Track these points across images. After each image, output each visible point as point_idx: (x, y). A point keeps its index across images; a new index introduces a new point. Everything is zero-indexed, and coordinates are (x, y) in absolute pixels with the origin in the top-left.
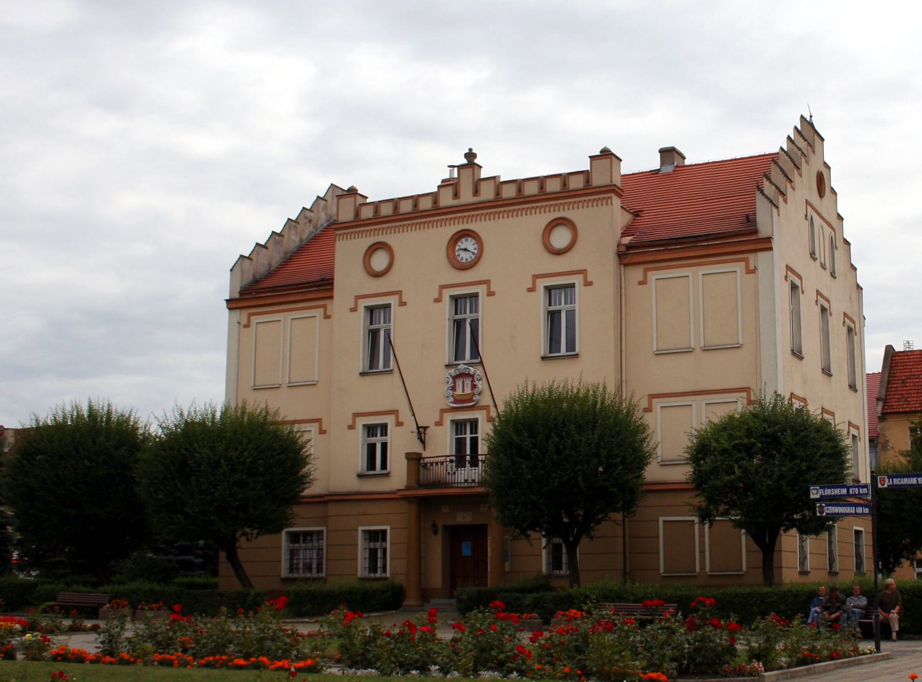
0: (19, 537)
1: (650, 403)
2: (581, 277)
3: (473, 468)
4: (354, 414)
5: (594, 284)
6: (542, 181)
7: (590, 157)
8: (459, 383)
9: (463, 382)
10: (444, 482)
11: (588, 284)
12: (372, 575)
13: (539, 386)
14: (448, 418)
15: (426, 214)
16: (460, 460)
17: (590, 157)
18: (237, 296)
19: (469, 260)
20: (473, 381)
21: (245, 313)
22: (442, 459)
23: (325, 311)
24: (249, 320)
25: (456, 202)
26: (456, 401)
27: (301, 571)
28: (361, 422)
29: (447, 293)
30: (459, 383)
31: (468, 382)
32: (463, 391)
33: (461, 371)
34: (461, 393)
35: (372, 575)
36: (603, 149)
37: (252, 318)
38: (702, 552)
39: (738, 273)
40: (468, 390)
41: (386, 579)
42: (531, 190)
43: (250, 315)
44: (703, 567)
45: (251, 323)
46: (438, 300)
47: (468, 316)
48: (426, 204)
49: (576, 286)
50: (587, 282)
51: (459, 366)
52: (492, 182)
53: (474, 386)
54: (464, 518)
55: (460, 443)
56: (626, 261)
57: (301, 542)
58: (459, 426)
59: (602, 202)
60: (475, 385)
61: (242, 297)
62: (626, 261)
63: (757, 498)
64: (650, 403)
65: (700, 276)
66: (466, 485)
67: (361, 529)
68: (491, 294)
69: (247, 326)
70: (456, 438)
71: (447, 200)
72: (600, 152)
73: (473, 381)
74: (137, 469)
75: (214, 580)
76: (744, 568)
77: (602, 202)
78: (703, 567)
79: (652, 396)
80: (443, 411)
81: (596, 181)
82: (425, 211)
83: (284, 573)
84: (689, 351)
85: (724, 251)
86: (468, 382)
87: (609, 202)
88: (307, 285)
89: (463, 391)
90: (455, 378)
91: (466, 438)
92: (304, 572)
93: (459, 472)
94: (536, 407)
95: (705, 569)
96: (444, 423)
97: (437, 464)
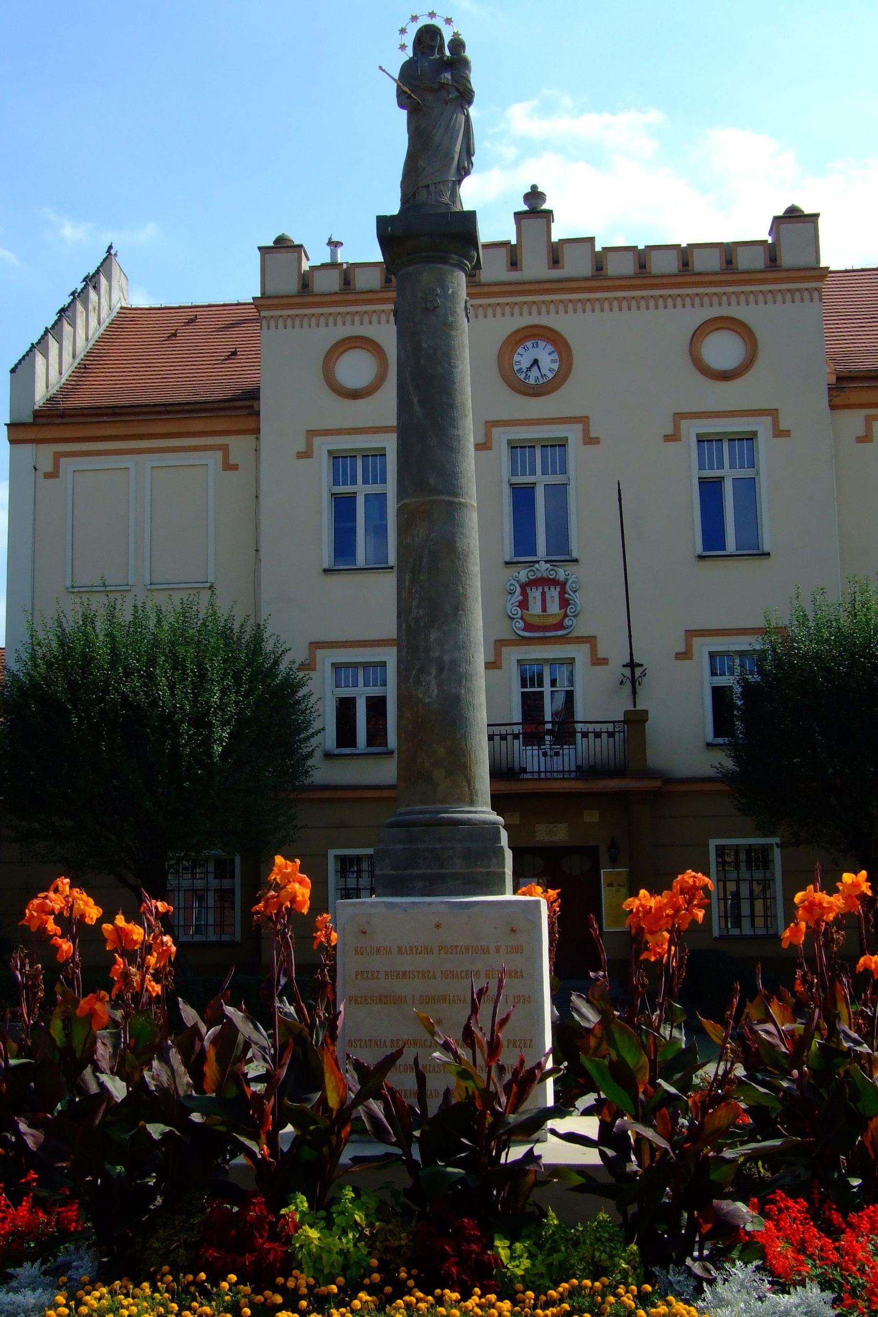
2: (768, 420)
3: (530, 748)
4: (311, 643)
7: (260, 248)
8: (535, 594)
9: (543, 594)
17: (260, 248)
20: (563, 592)
21: (47, 451)
23: (226, 456)
24: (56, 465)
29: (323, 446)
30: (535, 594)
31: (554, 593)
32: (544, 609)
33: (539, 575)
36: (279, 237)
40: (554, 608)
41: (232, 944)
43: (58, 456)
45: (62, 469)
47: (541, 481)
50: (590, 438)
51: (537, 565)
53: (564, 603)
56: (837, 401)
59: (302, 321)
62: (837, 401)
63: (49, 821)
67: (332, 853)
69: (54, 474)
70: (523, 693)
72: (274, 242)
73: (563, 592)
75: (459, 947)
77: (302, 321)
79: (316, 645)
81: (787, 259)
82: (662, 276)
86: (554, 593)
87: (816, 295)
88: (187, 407)
89: (544, 609)
91: (543, 692)
93: (566, 752)
94: (87, 660)
96: (318, 666)
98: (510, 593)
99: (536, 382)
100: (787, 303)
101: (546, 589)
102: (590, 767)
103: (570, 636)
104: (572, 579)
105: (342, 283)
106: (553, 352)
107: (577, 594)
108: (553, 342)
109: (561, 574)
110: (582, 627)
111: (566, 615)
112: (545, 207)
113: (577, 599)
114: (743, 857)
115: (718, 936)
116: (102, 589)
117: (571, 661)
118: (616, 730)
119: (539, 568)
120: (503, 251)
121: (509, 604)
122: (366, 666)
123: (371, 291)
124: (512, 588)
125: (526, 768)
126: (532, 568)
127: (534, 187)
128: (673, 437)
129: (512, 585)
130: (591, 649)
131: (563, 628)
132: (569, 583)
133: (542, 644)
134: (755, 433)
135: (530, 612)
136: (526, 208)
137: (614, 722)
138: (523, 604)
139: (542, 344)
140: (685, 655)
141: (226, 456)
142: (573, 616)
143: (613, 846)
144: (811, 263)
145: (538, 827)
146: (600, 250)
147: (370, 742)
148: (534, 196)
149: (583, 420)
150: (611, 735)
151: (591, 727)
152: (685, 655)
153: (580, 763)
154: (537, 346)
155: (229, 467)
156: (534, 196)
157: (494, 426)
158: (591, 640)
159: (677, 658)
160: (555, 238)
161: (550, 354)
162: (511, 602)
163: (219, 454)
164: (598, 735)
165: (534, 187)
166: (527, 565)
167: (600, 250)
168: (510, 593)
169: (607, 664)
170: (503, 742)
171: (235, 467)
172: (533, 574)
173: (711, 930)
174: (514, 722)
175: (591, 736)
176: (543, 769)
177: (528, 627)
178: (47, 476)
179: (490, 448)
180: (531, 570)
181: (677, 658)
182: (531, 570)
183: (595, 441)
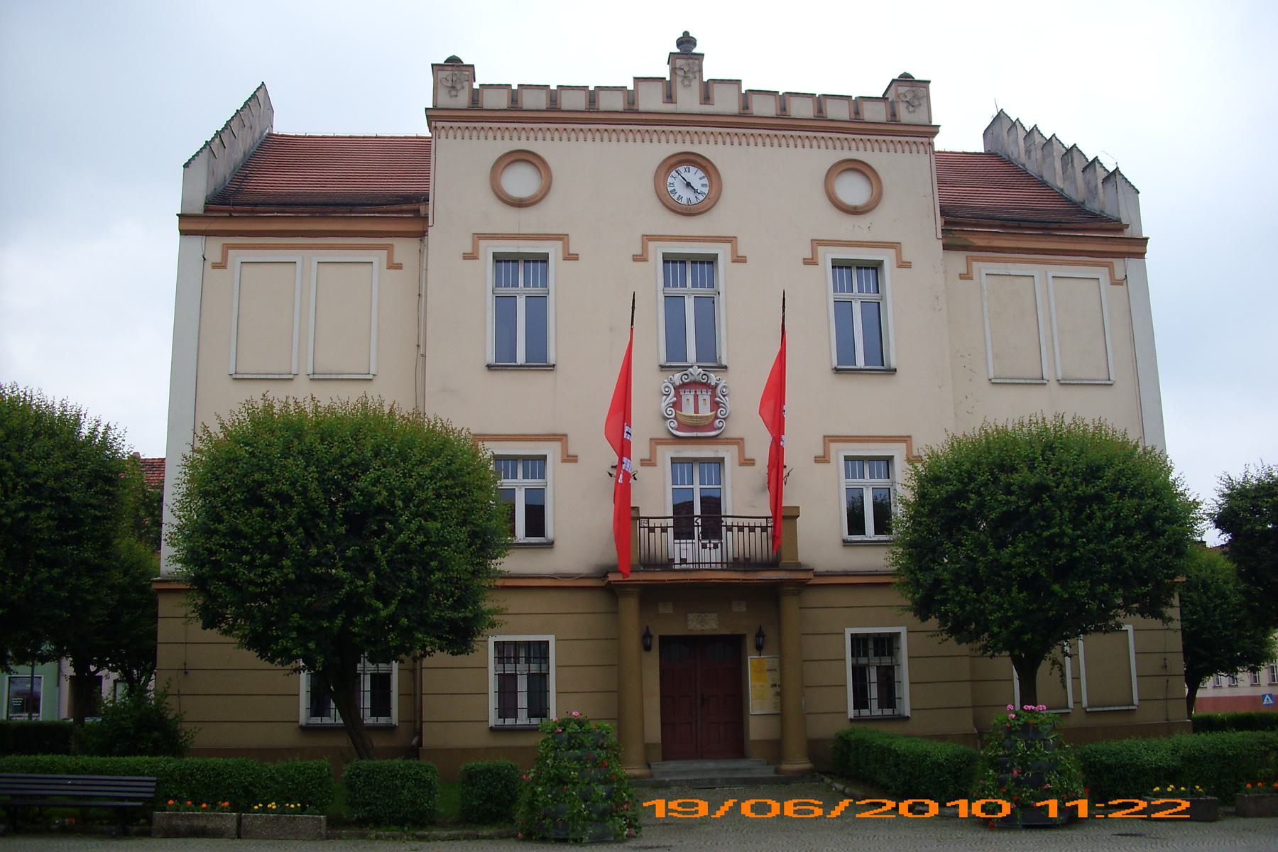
0: (310, 644)
2: (559, 244)
6: (820, 101)
8: (688, 397)
9: (696, 397)
12: (317, 720)
13: (226, 418)
16: (683, 528)
18: (198, 208)
19: (684, 201)
20: (714, 395)
21: (215, 245)
22: (752, 522)
24: (225, 256)
25: (669, 107)
27: (875, 704)
30: (688, 397)
31: (705, 397)
32: (696, 411)
35: (317, 720)
37: (231, 252)
38: (1076, 678)
40: (705, 411)
42: (803, 110)
43: (227, 248)
44: (1078, 702)
46: (640, 258)
49: (887, 266)
53: (715, 405)
54: (705, 624)
57: (871, 652)
60: (718, 403)
65: (315, 265)
66: (684, 566)
68: (739, 259)
71: (652, 101)
73: (714, 395)
76: (1136, 701)
78: (1078, 702)
80: (656, 442)
82: (563, 111)
83: (493, 720)
84: (1040, 383)
86: (705, 397)
89: (696, 411)
90: (684, 385)
92: (880, 706)
95: (1081, 703)
96: (659, 462)
97: (741, 529)
98: (665, 395)
99: (688, 203)
100: (750, 146)
101: (699, 393)
102: (745, 559)
103: (720, 437)
105: (510, 101)
106: (703, 177)
107: (726, 398)
109: (713, 379)
111: (716, 417)
112: (695, 51)
114: (871, 645)
115: (853, 717)
117: (544, 458)
118: (769, 525)
119: (693, 373)
120: (659, 85)
121: (663, 405)
122: (525, 459)
123: (538, 111)
124: (667, 389)
125: (686, 559)
126: (685, 372)
127: (686, 34)
128: (811, 261)
129: (667, 387)
130: (907, 447)
131: (715, 429)
132: (719, 388)
133: (692, 444)
134: (880, 263)
135: (682, 413)
136: (678, 51)
137: (767, 518)
138: (677, 405)
139: (693, 169)
140: (822, 459)
141: (390, 256)
142: (723, 419)
143: (760, 634)
144: (925, 121)
145: (691, 616)
146: (593, 89)
147: (529, 533)
148: (686, 41)
150: (764, 529)
152: (822, 459)
153: (736, 556)
154: (689, 171)
156: (686, 41)
158: (738, 442)
159: (816, 461)
160: (705, 79)
161: (700, 179)
162: (666, 403)
164: (752, 529)
165: (686, 34)
166: (681, 369)
167: (593, 89)
168: (665, 395)
169: (753, 464)
170: (741, 533)
171: (399, 267)
172: (686, 377)
173: (846, 712)
174: (668, 516)
175: (746, 530)
176: (725, 561)
178: (216, 266)
179: (476, 258)
180: (685, 374)
181: (816, 461)
182: (685, 374)
183: (575, 257)
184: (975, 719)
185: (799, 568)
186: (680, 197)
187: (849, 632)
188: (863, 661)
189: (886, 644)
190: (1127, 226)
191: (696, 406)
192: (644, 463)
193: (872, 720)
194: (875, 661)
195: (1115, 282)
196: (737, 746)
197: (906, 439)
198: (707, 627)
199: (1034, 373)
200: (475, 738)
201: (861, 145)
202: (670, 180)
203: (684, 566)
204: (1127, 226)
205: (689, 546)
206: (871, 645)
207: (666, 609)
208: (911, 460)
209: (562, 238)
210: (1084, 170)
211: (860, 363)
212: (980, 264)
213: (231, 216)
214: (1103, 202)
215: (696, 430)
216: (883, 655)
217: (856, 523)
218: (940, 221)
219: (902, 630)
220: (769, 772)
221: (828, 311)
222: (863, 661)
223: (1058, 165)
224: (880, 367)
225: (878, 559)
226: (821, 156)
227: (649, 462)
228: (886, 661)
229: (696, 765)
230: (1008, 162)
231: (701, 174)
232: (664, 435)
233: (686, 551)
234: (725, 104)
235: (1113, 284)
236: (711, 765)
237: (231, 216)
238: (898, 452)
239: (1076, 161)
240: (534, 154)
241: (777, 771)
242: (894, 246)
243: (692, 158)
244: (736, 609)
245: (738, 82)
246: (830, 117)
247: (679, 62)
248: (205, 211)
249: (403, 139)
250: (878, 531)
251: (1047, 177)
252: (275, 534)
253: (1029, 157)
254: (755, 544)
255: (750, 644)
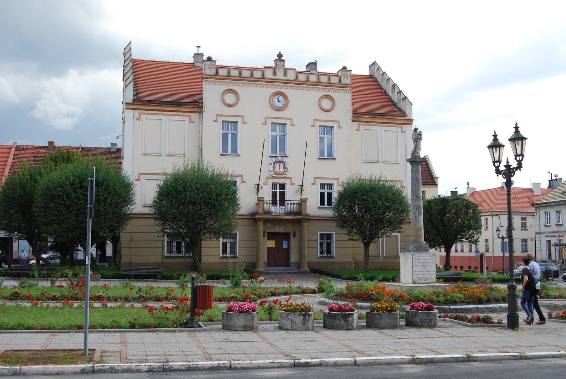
1: (139, 177)
5: (343, 128)
8: (277, 165)
9: (279, 165)
10: (269, 211)
11: (340, 127)
12: (169, 255)
14: (271, 181)
15: (258, 80)
16: (274, 203)
20: (284, 165)
22: (294, 202)
24: (140, 116)
25: (274, 77)
26: (275, 174)
27: (325, 253)
28: (319, 182)
29: (270, 121)
30: (277, 165)
31: (282, 165)
32: (279, 169)
34: (278, 170)
37: (142, 115)
38: (383, 248)
39: (186, 121)
40: (282, 170)
44: (383, 255)
46: (264, 124)
48: (257, 74)
52: (294, 71)
53: (285, 168)
55: (274, 195)
57: (325, 239)
58: (274, 186)
60: (285, 167)
61: (134, 103)
64: (139, 177)
66: (275, 214)
68: (293, 125)
69: (138, 119)
71: (269, 74)
73: (284, 165)
74: (227, 195)
78: (383, 255)
79: (140, 174)
80: (267, 178)
82: (243, 77)
83: (221, 255)
84: (159, 155)
85: (138, 108)
86: (282, 165)
89: (279, 169)
90: (276, 162)
97: (291, 204)
104: (287, 162)
108: (284, 97)
109: (284, 160)
110: (288, 175)
113: (288, 167)
114: (325, 236)
116: (183, 155)
131: (284, 175)
132: (286, 163)
136: (277, 58)
138: (274, 168)
140: (314, 184)
141: (190, 119)
143: (295, 233)
148: (280, 55)
149: (291, 119)
151: (290, 202)
152: (314, 184)
155: (191, 122)
156: (280, 55)
157: (268, 118)
158: (291, 178)
163: (188, 118)
164: (294, 204)
171: (193, 122)
173: (318, 255)
177: (275, 174)
178: (137, 119)
183: (245, 123)
184: (353, 258)
185: (307, 215)
186: (276, 105)
187: (319, 233)
188: (323, 241)
189: (329, 237)
190: (408, 115)
191: (280, 169)
192: (264, 184)
193: (324, 257)
194: (326, 241)
195: (402, 132)
196: (287, 263)
197: (338, 179)
198: (280, 230)
199: (376, 159)
200: (216, 260)
201: (330, 90)
202: (274, 100)
203: (275, 214)
204: (408, 115)
205: (275, 207)
206: (325, 236)
207: (269, 225)
208: (339, 185)
209: (242, 117)
210: (398, 93)
211: (326, 156)
212: (362, 126)
213: (142, 104)
214: (401, 105)
215: (278, 175)
216: (328, 239)
217: (322, 203)
218: (351, 113)
219: (334, 233)
220: (296, 271)
221: (317, 141)
222: (323, 241)
223: (391, 88)
224: (331, 157)
225: (330, 213)
226: (317, 94)
227: (265, 183)
228: (329, 241)
229: (277, 268)
230: (375, 81)
231: (283, 98)
232: (270, 176)
233: (274, 209)
234: (291, 76)
235: (402, 133)
236: (281, 268)
237: (143, 104)
238: (335, 182)
239: (396, 89)
240: (233, 90)
241: (299, 271)
242: (338, 122)
243: (280, 93)
244: (268, 225)
245: (295, 69)
246: (321, 81)
247: (278, 63)
248: (133, 102)
249: (176, 64)
250: (328, 205)
251: (387, 91)
252: (448, 251)
253: (382, 82)
254: (294, 208)
255: (292, 235)
